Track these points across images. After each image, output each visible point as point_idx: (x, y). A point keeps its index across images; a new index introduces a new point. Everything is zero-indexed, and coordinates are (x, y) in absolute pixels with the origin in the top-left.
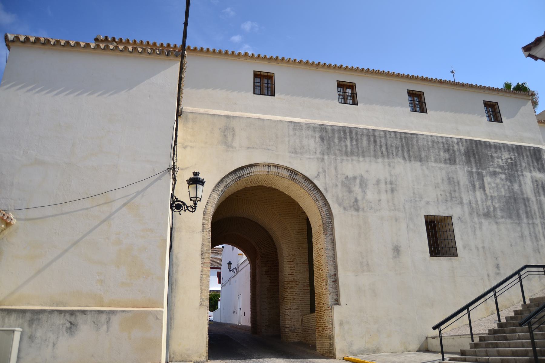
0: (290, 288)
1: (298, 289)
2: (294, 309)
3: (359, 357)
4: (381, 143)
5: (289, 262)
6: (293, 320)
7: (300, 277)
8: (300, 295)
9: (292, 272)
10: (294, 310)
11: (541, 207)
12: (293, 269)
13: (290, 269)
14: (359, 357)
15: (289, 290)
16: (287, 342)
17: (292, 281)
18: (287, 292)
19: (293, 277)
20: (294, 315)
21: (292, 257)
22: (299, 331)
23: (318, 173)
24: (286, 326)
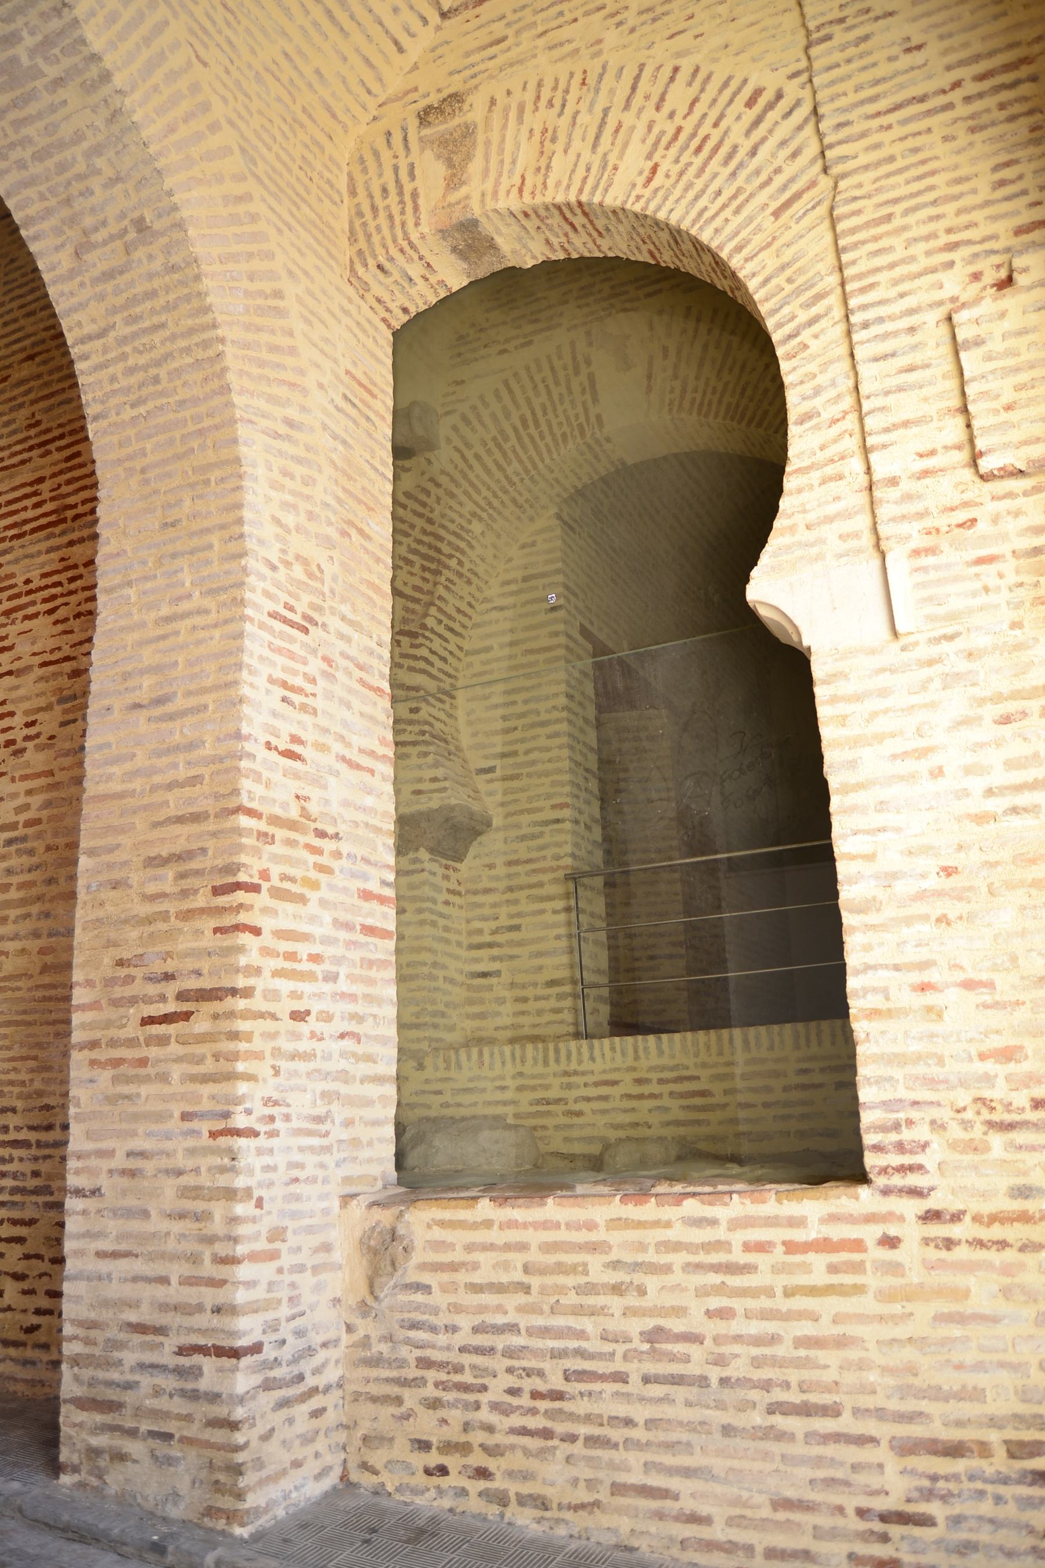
0: (277, 893)
1: (327, 917)
2: (295, 1124)
3: (573, 171)
4: (855, 1213)
5: (278, 626)
6: (286, 1260)
7: (346, 803)
8: (343, 985)
9: (295, 730)
10: (299, 1132)
11: (552, 5)
12: (304, 708)
13: (284, 700)
14: (573, 171)
15: (265, 910)
16: (238, 1531)
17: (292, 825)
18: (256, 931)
19: (295, 786)
20: (298, 1198)
21: (299, 584)
22: (332, 1375)
23: (431, 118)
24: (233, 1334)
